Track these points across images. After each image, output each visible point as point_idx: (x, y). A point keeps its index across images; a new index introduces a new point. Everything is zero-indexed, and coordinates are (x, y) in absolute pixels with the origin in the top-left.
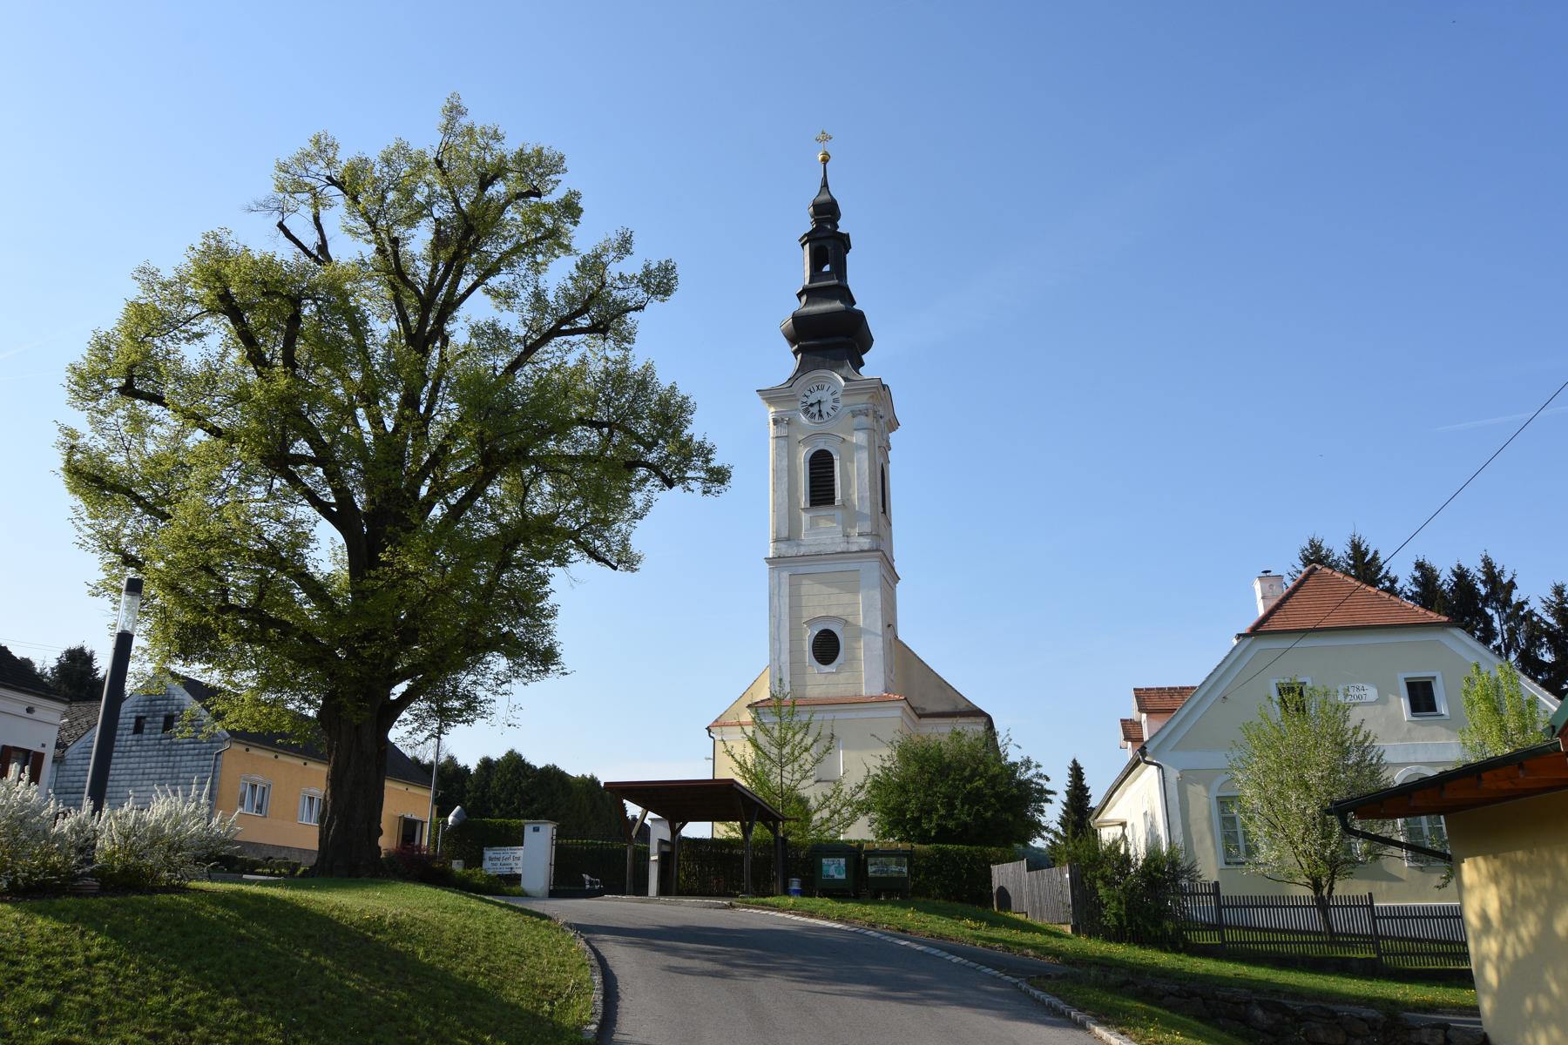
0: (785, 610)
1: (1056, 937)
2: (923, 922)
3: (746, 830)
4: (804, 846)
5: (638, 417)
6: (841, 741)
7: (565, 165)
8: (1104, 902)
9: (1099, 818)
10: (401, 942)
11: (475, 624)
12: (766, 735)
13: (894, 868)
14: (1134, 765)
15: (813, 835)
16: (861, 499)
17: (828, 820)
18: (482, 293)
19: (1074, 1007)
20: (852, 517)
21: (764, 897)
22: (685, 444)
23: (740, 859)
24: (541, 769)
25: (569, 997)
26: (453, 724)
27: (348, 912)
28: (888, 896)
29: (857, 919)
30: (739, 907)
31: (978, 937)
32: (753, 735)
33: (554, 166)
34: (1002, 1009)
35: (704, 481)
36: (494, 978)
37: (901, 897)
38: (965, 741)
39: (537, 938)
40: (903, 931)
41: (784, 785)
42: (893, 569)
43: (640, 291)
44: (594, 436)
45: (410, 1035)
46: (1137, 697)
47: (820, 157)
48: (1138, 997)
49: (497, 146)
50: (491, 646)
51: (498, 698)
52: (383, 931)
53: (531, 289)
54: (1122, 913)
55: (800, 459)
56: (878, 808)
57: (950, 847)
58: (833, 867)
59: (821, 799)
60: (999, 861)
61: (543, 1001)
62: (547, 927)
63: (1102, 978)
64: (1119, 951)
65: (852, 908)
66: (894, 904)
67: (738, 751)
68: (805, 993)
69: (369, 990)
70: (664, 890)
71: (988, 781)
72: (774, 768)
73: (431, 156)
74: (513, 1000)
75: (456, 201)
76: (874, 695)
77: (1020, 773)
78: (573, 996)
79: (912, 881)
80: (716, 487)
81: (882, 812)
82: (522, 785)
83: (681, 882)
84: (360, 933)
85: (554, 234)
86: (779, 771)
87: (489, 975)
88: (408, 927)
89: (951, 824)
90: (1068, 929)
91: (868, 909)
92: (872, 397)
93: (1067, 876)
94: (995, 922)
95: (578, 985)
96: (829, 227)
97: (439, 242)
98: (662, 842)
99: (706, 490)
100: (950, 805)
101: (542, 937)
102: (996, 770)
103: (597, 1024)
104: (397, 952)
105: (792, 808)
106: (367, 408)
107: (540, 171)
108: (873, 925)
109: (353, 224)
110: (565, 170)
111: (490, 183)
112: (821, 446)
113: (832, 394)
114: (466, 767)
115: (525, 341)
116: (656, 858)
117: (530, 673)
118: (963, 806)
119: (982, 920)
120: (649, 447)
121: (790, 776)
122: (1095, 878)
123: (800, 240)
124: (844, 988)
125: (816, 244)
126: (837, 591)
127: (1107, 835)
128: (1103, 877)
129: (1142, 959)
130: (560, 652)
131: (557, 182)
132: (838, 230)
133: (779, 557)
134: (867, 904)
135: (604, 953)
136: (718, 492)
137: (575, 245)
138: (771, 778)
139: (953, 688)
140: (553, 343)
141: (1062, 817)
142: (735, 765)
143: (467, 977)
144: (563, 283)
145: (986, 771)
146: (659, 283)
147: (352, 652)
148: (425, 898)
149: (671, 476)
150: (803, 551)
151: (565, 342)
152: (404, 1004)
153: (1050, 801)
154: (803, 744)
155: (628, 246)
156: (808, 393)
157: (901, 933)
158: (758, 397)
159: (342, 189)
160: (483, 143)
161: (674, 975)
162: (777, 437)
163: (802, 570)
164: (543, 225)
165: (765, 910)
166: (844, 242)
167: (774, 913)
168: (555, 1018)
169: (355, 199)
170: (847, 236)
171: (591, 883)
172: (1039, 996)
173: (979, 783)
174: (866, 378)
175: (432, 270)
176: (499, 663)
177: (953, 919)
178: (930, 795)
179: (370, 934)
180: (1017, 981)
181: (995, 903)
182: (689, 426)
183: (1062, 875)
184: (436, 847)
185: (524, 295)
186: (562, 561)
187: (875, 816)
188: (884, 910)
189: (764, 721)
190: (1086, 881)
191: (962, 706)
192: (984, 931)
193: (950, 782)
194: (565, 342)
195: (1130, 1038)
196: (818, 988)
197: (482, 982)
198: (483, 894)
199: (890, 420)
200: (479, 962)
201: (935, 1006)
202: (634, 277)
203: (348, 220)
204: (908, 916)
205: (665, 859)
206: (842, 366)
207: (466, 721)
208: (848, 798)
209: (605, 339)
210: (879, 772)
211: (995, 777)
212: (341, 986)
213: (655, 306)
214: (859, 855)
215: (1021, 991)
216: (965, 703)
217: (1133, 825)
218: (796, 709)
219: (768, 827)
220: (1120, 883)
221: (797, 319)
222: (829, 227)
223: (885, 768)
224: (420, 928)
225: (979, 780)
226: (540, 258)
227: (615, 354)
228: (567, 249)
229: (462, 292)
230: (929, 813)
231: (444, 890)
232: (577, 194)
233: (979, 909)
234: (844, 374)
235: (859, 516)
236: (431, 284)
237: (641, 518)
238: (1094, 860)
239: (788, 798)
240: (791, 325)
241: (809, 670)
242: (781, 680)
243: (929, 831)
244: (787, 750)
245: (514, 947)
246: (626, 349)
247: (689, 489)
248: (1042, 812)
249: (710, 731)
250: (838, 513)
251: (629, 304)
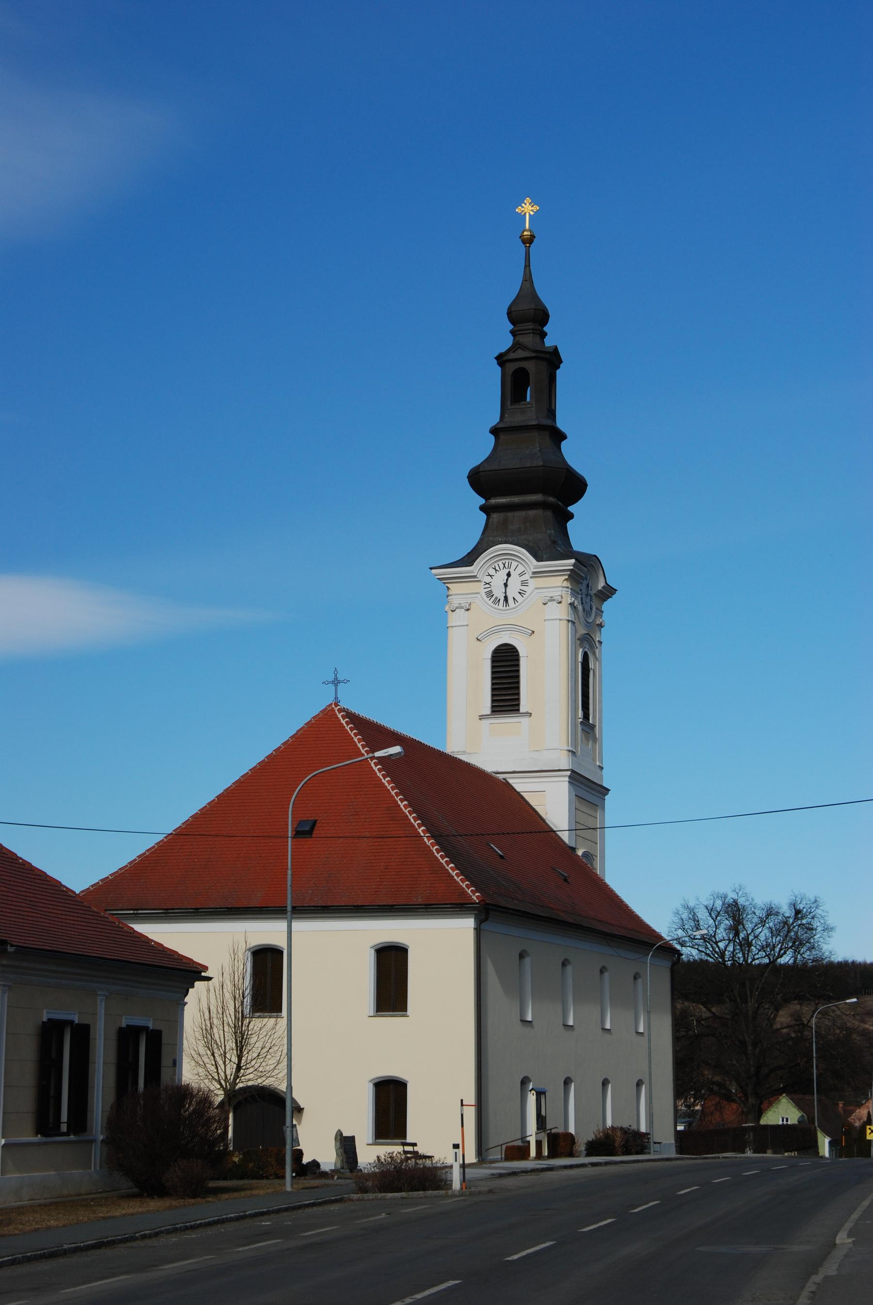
156: (492, 572)
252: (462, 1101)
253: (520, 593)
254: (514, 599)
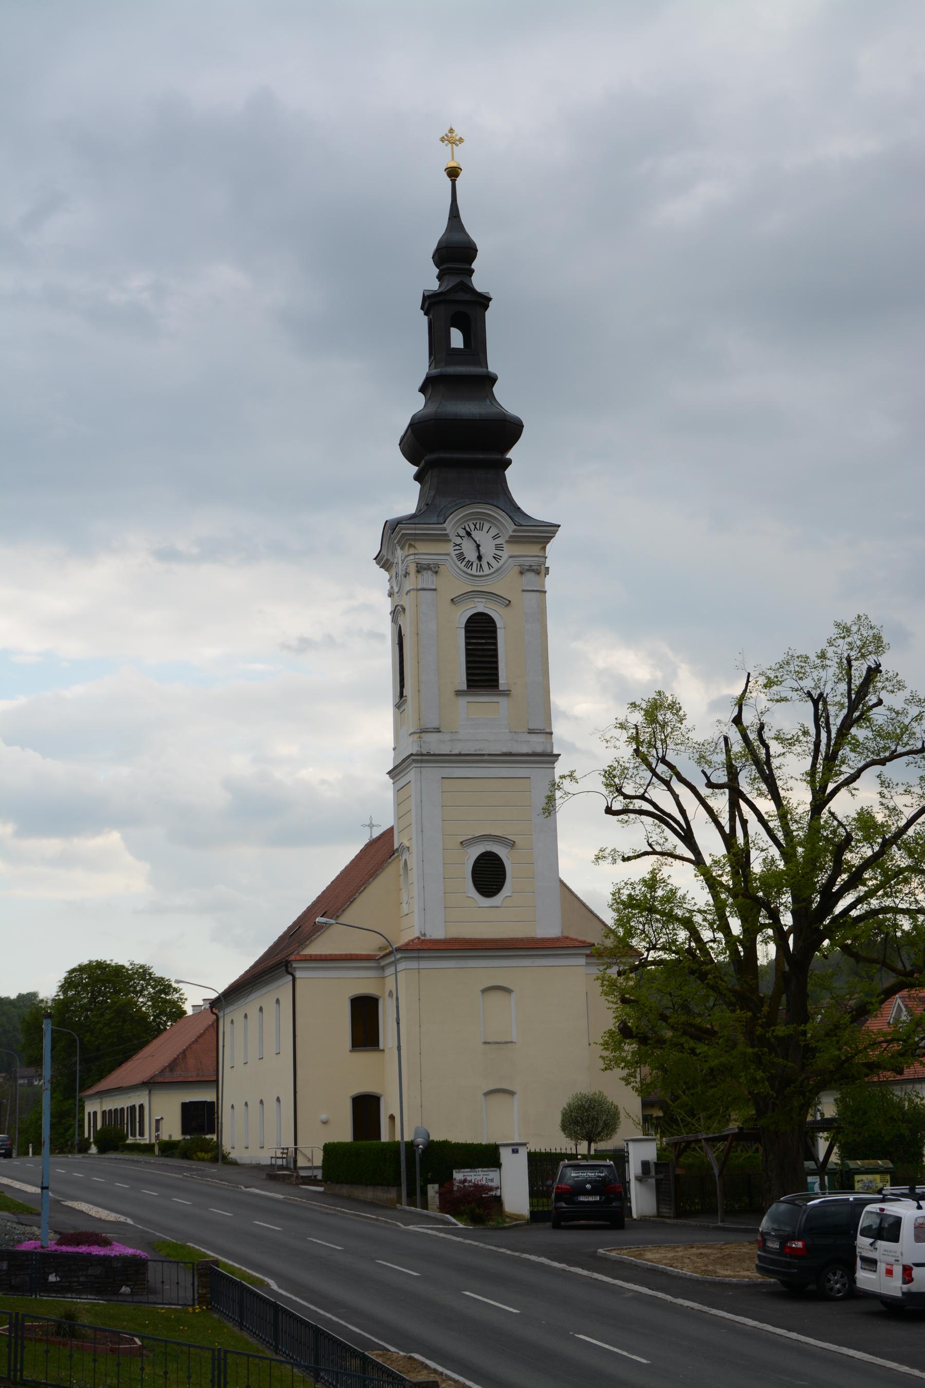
112: (481, 609)
253: (494, 557)
254: (488, 563)
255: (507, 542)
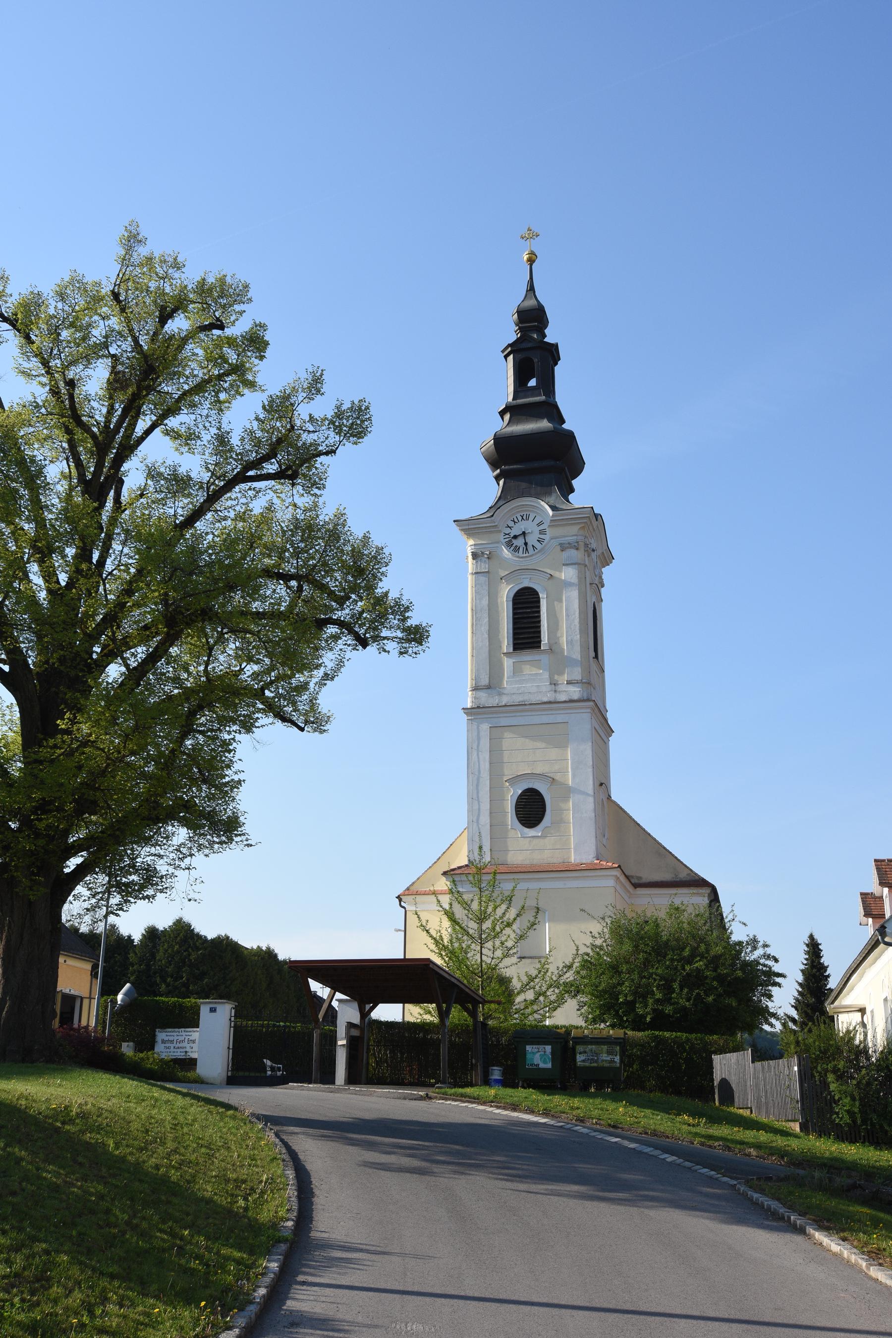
0: (485, 766)
1: (781, 1135)
2: (636, 1117)
3: (443, 1014)
4: (506, 1032)
5: (329, 572)
6: (547, 913)
7: (249, 295)
8: (836, 1098)
9: (836, 1003)
10: (90, 1132)
11: (156, 795)
12: (465, 908)
13: (605, 1057)
14: (872, 946)
15: (515, 1019)
16: (570, 642)
17: (533, 1002)
18: (161, 434)
19: (794, 1211)
20: (559, 663)
21: (462, 1087)
22: (380, 601)
23: (436, 1044)
24: (213, 940)
25: (263, 1193)
26: (132, 900)
27: (34, 1101)
28: (600, 1087)
29: (564, 1113)
30: (436, 1098)
31: (696, 1134)
32: (451, 908)
33: (239, 295)
34: (719, 1212)
35: (401, 640)
36: (186, 1172)
37: (613, 1089)
38: (685, 918)
39: (224, 1130)
40: (614, 1127)
41: (483, 963)
42: (606, 720)
43: (332, 434)
44: (281, 590)
45: (110, 1228)
46: (879, 869)
47: (526, 257)
48: (865, 1202)
49: (177, 275)
50: (170, 816)
51: (177, 873)
52: (72, 1121)
53: (214, 431)
54: (856, 1110)
55: (502, 597)
56: (587, 990)
57: (667, 1034)
58: (538, 1055)
59: (525, 979)
60: (722, 1051)
61: (237, 1196)
62: (234, 1118)
63: (827, 1181)
64: (851, 1151)
65: (558, 1101)
66: (605, 1097)
67: (433, 927)
68: (508, 1191)
69: (66, 1182)
70: (353, 1078)
71: (710, 962)
72: (473, 945)
73: (106, 289)
74: (208, 1195)
75: (136, 340)
76: (584, 861)
77: (746, 953)
78: (267, 1191)
79: (625, 1071)
80: (413, 647)
81: (592, 995)
82: (191, 958)
83: (371, 1069)
84: (49, 1124)
85: (238, 369)
86: (479, 948)
87: (180, 1168)
88: (95, 1118)
89: (668, 1009)
90: (796, 1127)
91: (576, 1102)
92: (583, 528)
93: (796, 1068)
94: (715, 1119)
95: (271, 1181)
96: (535, 336)
97: (116, 383)
98: (350, 1025)
99: (403, 650)
100: (667, 988)
101: (229, 1129)
102: (718, 950)
103: (293, 1220)
104: (87, 1143)
105: (493, 989)
106: (41, 562)
107: (223, 301)
108: (581, 1120)
109: (26, 365)
110: (250, 300)
111: (171, 316)
112: (526, 584)
113: (538, 525)
114: (129, 937)
115: (208, 488)
116: (344, 1042)
117: (211, 844)
118: (681, 990)
119: (701, 1115)
120: (341, 601)
121: (490, 954)
122: (826, 1071)
123: (503, 351)
124: (550, 1187)
125: (520, 356)
126: (543, 745)
127: (845, 1022)
128: (835, 1071)
129: (876, 1161)
130: (244, 821)
131: (241, 313)
132: (546, 340)
133: (478, 707)
134: (575, 1096)
135: (295, 1147)
136: (416, 653)
137: (260, 380)
138: (469, 955)
139: (673, 855)
140: (237, 489)
141: (797, 1000)
142: (430, 942)
143: (159, 1170)
144: (248, 426)
145: (707, 951)
146: (352, 424)
147: (26, 823)
148: (106, 1086)
149: (365, 635)
150: (505, 700)
151: (250, 489)
152: (101, 1197)
153: (779, 985)
154: (505, 919)
155: (319, 385)
156: (511, 524)
157: (612, 1130)
158: (455, 528)
159: (14, 326)
160: (162, 272)
161: (370, 1171)
162: (476, 573)
163: (504, 722)
164: (226, 361)
165: (464, 1102)
166: (552, 354)
167: (474, 1105)
168: (250, 1214)
169: (27, 337)
170: (556, 346)
171: (272, 1069)
172: (757, 1199)
173: (699, 964)
174: (577, 506)
175: (108, 412)
176: (181, 834)
177: (670, 1114)
178: (645, 977)
179: (59, 1124)
180: (735, 1182)
181: (716, 1096)
182: (384, 579)
183: (790, 1067)
184: (104, 1028)
185: (206, 437)
186: (248, 726)
187: (585, 999)
188: (593, 1104)
189: (460, 890)
190: (816, 1075)
191: (683, 875)
192: (703, 1128)
193: (668, 963)
194: (250, 489)
195: (852, 1244)
196: (522, 1186)
197: (174, 1175)
198: (163, 1081)
199: (603, 553)
200: (169, 1154)
201: (647, 1207)
202: (323, 420)
203: (21, 361)
204: (620, 1111)
205: (354, 1045)
206: (549, 494)
207: (148, 897)
208: (555, 979)
209: (293, 485)
210: (589, 951)
211: (717, 958)
212: (39, 1177)
213: (347, 450)
214: (567, 1042)
215: (739, 1194)
216: (686, 872)
217: (872, 1012)
218: (498, 877)
219: (466, 1009)
220: (854, 1078)
221: (500, 441)
222: (535, 336)
223: (596, 946)
224: (107, 1118)
225: (700, 960)
226: (223, 396)
227: (304, 501)
228: (251, 385)
229: (139, 434)
230: (644, 996)
231: (124, 1078)
232: (262, 326)
233: (698, 1103)
234: (552, 502)
235: (566, 662)
236: (107, 426)
237: (332, 679)
238: (824, 1052)
239: (488, 978)
240: (496, 456)
241: (512, 834)
242: (480, 848)
243: (643, 1017)
244: (487, 925)
245: (202, 1139)
246: (315, 495)
247: (385, 651)
248: (770, 996)
249: (400, 900)
250: (545, 659)
251: (320, 448)
252: (245, 311)
254: (533, 546)
255: (549, 526)
